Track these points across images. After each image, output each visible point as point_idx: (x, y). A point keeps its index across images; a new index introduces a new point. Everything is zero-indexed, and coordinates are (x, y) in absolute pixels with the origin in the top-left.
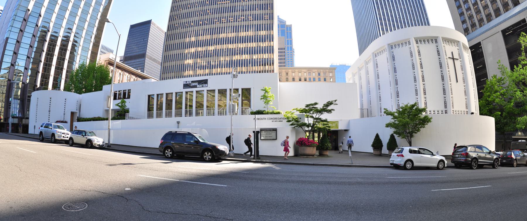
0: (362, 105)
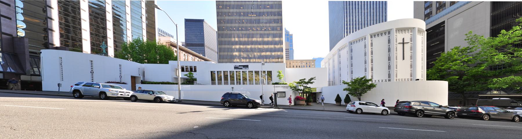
0: (329, 79)
